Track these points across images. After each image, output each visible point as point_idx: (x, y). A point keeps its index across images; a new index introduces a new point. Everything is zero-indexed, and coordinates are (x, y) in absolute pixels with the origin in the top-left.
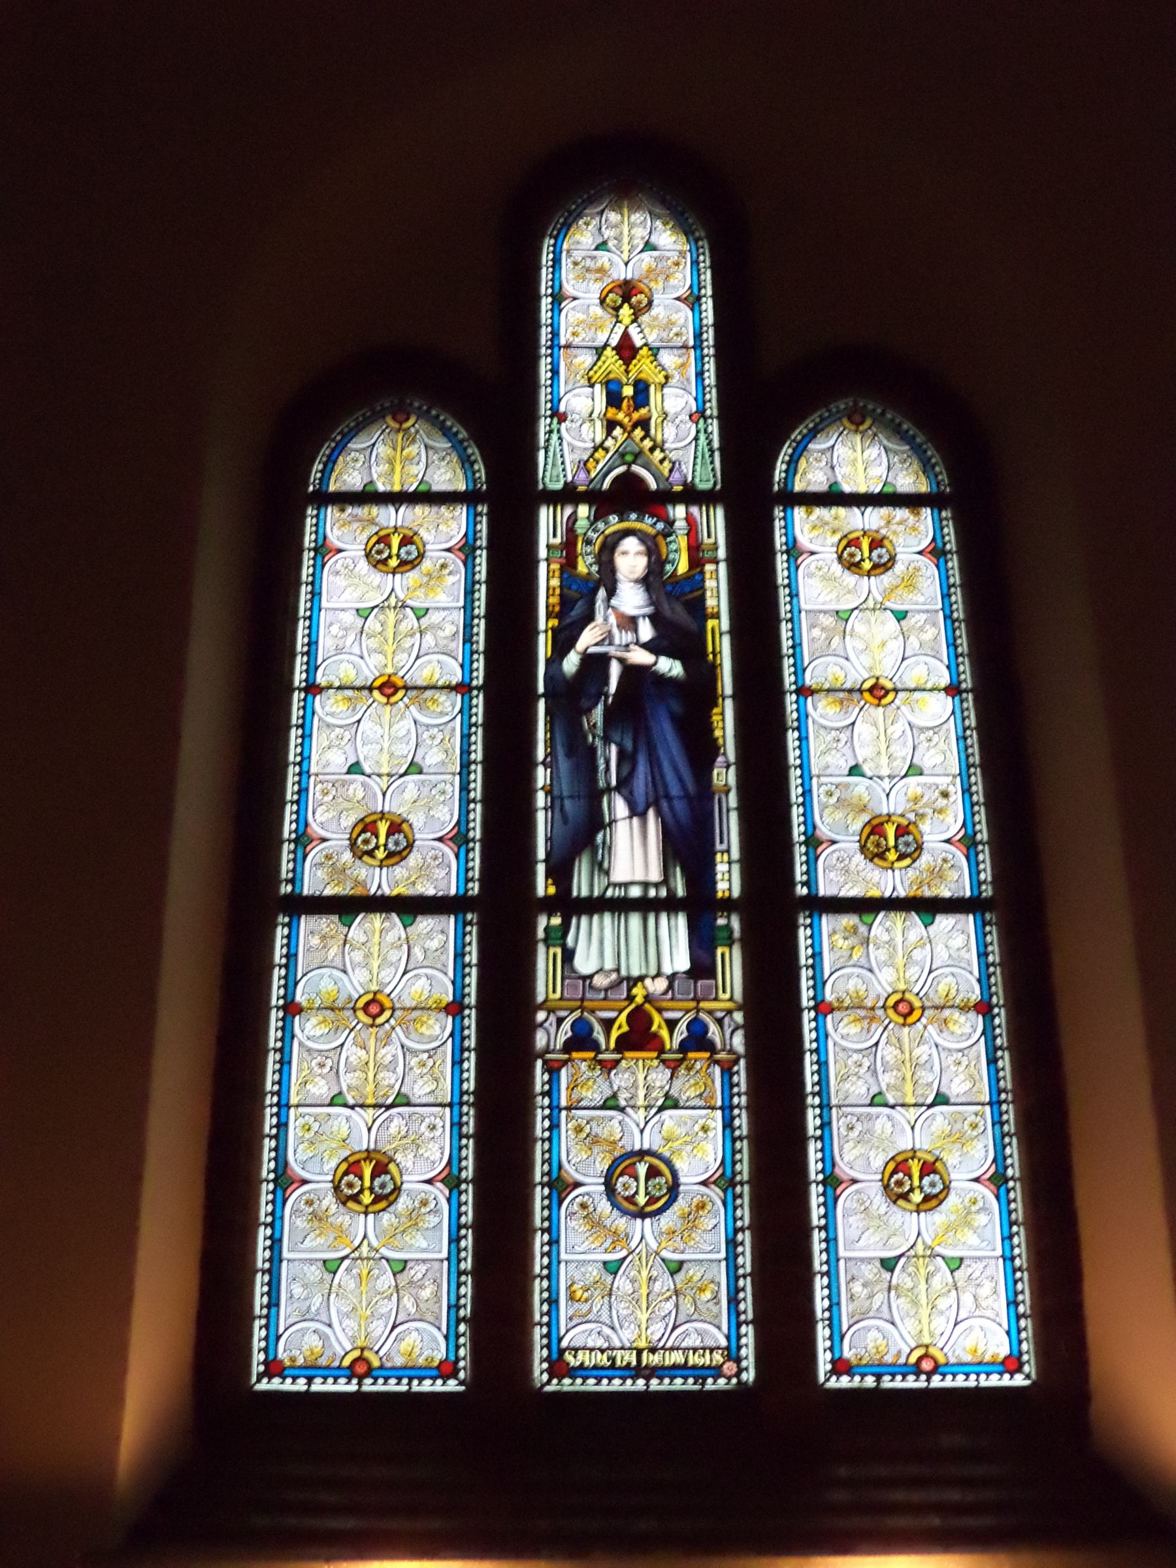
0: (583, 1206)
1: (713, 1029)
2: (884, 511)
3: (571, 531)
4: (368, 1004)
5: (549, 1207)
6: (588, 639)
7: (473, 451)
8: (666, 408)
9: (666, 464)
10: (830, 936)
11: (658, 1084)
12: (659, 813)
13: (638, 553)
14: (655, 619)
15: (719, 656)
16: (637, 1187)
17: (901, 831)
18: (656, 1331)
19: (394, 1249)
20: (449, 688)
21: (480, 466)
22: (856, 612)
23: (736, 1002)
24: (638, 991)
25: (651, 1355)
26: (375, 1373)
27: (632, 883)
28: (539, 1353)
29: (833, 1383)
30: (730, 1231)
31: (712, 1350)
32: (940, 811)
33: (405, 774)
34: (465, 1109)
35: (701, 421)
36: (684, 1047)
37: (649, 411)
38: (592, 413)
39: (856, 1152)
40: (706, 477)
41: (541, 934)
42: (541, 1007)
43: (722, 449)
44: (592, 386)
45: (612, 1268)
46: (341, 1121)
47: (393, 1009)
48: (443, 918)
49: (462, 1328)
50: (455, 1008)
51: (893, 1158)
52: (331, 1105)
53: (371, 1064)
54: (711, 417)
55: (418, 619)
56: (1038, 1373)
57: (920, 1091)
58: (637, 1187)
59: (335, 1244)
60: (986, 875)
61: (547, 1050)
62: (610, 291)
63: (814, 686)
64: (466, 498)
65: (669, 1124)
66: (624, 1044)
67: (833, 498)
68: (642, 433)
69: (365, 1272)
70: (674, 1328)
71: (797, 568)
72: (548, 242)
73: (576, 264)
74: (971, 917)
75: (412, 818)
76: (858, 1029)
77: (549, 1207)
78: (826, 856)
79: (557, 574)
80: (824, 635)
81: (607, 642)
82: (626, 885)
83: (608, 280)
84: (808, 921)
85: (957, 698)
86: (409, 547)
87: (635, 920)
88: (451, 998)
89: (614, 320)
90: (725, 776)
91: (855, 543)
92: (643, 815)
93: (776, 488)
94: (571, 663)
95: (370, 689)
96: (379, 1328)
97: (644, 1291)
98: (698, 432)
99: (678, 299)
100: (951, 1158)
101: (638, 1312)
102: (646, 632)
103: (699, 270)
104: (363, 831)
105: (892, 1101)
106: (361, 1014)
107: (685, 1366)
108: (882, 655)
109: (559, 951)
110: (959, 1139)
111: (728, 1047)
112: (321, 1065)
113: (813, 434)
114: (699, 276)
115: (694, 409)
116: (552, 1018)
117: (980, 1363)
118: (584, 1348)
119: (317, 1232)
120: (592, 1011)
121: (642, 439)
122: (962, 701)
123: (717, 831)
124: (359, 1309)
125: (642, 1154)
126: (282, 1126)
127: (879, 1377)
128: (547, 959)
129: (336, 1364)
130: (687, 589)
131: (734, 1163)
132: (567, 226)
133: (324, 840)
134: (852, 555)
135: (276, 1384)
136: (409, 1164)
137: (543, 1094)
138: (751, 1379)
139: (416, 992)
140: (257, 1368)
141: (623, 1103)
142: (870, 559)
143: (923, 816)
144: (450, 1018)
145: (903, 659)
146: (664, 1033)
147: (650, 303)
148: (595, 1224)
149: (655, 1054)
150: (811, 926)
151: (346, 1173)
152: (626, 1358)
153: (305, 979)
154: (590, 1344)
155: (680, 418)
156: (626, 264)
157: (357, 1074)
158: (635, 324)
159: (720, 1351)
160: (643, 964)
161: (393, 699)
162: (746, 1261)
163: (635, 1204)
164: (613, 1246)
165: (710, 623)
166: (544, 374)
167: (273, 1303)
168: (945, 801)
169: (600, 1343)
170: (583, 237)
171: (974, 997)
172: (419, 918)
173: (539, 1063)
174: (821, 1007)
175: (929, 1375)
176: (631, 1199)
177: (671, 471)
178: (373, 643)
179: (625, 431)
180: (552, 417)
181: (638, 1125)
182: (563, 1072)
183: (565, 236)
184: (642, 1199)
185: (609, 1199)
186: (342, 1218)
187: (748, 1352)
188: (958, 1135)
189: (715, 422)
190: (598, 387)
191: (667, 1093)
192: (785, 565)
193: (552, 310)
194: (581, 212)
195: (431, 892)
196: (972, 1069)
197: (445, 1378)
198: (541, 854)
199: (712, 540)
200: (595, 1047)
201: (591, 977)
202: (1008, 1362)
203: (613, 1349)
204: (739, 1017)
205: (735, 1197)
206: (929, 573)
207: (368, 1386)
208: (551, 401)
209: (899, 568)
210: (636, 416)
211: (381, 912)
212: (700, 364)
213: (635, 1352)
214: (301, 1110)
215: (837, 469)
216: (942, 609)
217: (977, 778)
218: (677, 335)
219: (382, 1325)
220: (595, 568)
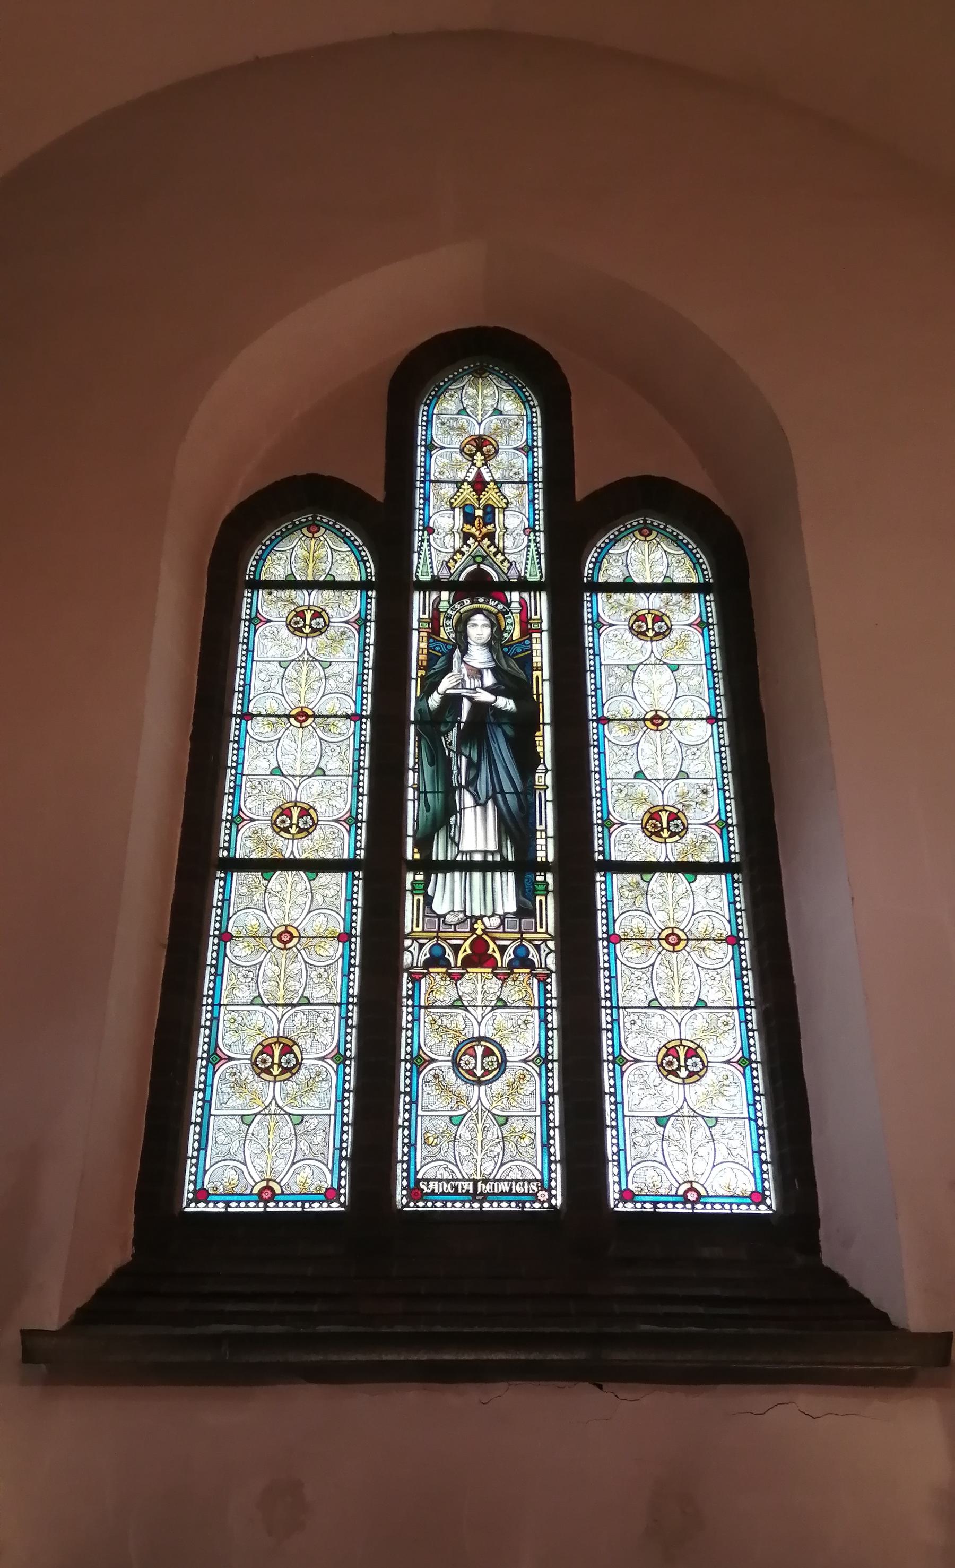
0: (436, 1076)
1: (533, 951)
2: (664, 596)
3: (436, 612)
5: (411, 1078)
6: (446, 684)
7: (366, 552)
8: (506, 525)
9: (506, 564)
10: (619, 889)
12: (496, 803)
13: (484, 625)
15: (541, 696)
16: (476, 1064)
17: (673, 817)
18: (488, 1167)
19: (294, 1107)
20: (347, 716)
21: (370, 564)
22: (641, 666)
24: (479, 926)
25: (484, 1185)
26: (277, 1198)
27: (477, 851)
28: (400, 1183)
29: (621, 1208)
30: (544, 1095)
31: (529, 1181)
32: (702, 803)
33: (313, 775)
34: (350, 1007)
35: (532, 534)
36: (511, 966)
37: (495, 527)
38: (453, 528)
39: (637, 1041)
41: (409, 886)
42: (407, 937)
43: (547, 554)
44: (453, 509)
45: (456, 1121)
46: (258, 1016)
48: (338, 875)
49: (344, 1164)
51: (664, 1046)
52: (252, 1004)
53: (282, 976)
54: (539, 531)
55: (324, 669)
56: (777, 1206)
59: (250, 1104)
60: (736, 848)
61: (412, 967)
62: (467, 444)
64: (362, 586)
65: (499, 1018)
66: (468, 962)
67: (628, 587)
68: (489, 543)
69: (272, 1124)
70: (502, 1165)
71: (599, 635)
73: (443, 424)
74: (723, 876)
75: (317, 806)
76: (639, 954)
77: (411, 1078)
78: (616, 833)
79: (425, 639)
80: (617, 682)
81: (460, 687)
82: (471, 853)
83: (465, 436)
84: (603, 879)
86: (285, 1066)
87: (477, 876)
88: (342, 931)
89: (470, 463)
90: (545, 778)
91: (643, 618)
92: (484, 805)
93: (585, 580)
94: (434, 701)
95: (288, 717)
96: (281, 1165)
97: (480, 1138)
98: (529, 541)
99: (516, 449)
100: (708, 1046)
102: (489, 680)
103: (533, 427)
104: (281, 815)
105: (664, 1005)
106: (275, 941)
107: (510, 1193)
108: (660, 695)
109: (421, 898)
110: (715, 1034)
111: (543, 966)
112: (246, 977)
113: (615, 541)
114: (533, 431)
115: (527, 526)
116: (416, 945)
117: (732, 1196)
118: (434, 1180)
119: (238, 1095)
121: (489, 546)
122: (719, 727)
124: (267, 1151)
125: (480, 1039)
126: (215, 1019)
127: (655, 1204)
128: (413, 902)
129: (248, 1192)
130: (519, 650)
132: (438, 396)
133: (252, 820)
134: (640, 627)
135: (201, 1207)
136: (308, 1047)
137: (408, 997)
142: (653, 629)
143: (688, 806)
145: (676, 698)
146: (497, 955)
147: (497, 452)
148: (444, 1089)
149: (490, 970)
150: (605, 882)
151: (261, 1053)
152: (466, 1187)
153: (235, 916)
154: (439, 1177)
155: (516, 532)
156: (480, 424)
158: (485, 467)
159: (535, 1183)
160: (482, 907)
161: (304, 724)
162: (556, 1117)
163: (475, 1075)
164: (456, 1105)
165: (535, 674)
166: (419, 501)
167: (203, 1147)
168: (705, 797)
169: (446, 1176)
170: (448, 406)
171: (725, 933)
172: (320, 875)
173: (405, 975)
174: (612, 939)
175: (694, 1203)
176: (471, 1072)
177: (509, 569)
178: (290, 686)
179: (476, 541)
180: (423, 531)
181: (477, 1020)
182: (423, 981)
183: (435, 405)
184: (479, 1072)
186: (258, 1085)
187: (557, 1184)
188: (713, 1030)
189: (542, 535)
190: (457, 510)
191: (499, 997)
192: (591, 634)
193: (425, 457)
195: (330, 857)
198: (410, 831)
199: (538, 617)
200: (447, 964)
201: (444, 916)
202: (754, 1197)
203: (458, 1180)
204: (551, 944)
205: (548, 1070)
207: (272, 1207)
208: (423, 520)
209: (674, 635)
210: (484, 530)
213: (471, 1183)
214: (228, 1008)
215: (630, 568)
217: (729, 780)
219: (284, 1163)
220: (453, 635)
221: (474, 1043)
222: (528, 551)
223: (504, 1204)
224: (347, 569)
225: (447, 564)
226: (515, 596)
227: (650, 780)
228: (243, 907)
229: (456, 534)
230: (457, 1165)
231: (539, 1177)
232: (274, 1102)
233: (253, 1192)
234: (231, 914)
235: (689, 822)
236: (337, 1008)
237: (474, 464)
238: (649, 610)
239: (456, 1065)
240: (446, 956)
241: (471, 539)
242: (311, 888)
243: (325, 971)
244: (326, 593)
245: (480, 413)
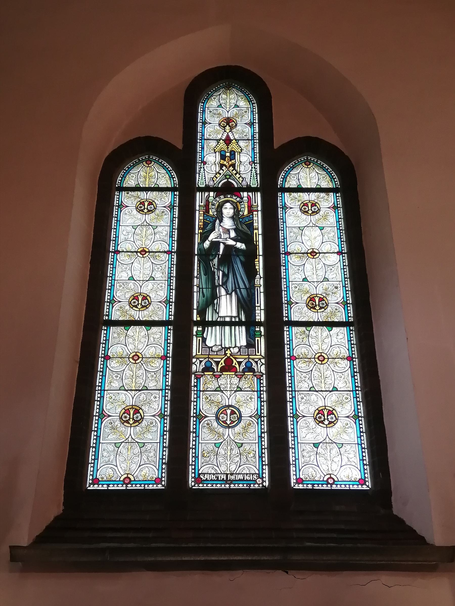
0: (208, 424)
1: (254, 364)
3: (207, 201)
4: (133, 356)
6: (212, 237)
7: (174, 173)
9: (241, 179)
11: (234, 383)
12: (236, 293)
13: (230, 208)
14: (236, 230)
17: (321, 300)
18: (233, 467)
19: (140, 439)
20: (165, 252)
21: (176, 179)
22: (306, 228)
23: (262, 356)
24: (228, 352)
26: (132, 482)
27: (227, 316)
28: (191, 475)
29: (296, 487)
30: (260, 433)
31: (253, 474)
32: (335, 293)
36: (244, 371)
37: (235, 161)
38: (215, 162)
39: (304, 407)
40: (254, 184)
41: (195, 333)
42: (194, 357)
44: (215, 153)
45: (217, 445)
46: (123, 396)
47: (143, 358)
48: (161, 328)
52: (120, 390)
53: (134, 376)
54: (257, 163)
55: (154, 229)
57: (327, 386)
60: (351, 314)
63: (291, 252)
66: (223, 369)
67: (299, 190)
68: (233, 169)
69: (130, 447)
72: (201, 104)
73: (210, 112)
74: (345, 328)
75: (151, 295)
82: (224, 317)
83: (221, 118)
84: (288, 329)
85: (341, 256)
86: (151, 206)
87: (227, 328)
90: (260, 281)
91: (306, 205)
92: (231, 294)
94: (207, 244)
95: (137, 252)
96: (134, 467)
97: (229, 454)
98: (252, 168)
99: (246, 124)
100: (338, 409)
101: (227, 461)
102: (233, 234)
103: (253, 113)
104: (133, 299)
107: (243, 480)
108: (315, 242)
109: (201, 339)
112: (117, 377)
116: (198, 361)
117: (350, 481)
118: (207, 474)
121: (232, 171)
122: (343, 256)
125: (229, 406)
126: (102, 397)
129: (118, 479)
130: (247, 220)
131: (261, 409)
133: (120, 302)
134: (305, 209)
135: (96, 487)
136: (147, 410)
138: (267, 485)
139: (151, 352)
140: (89, 481)
141: (222, 389)
142: (311, 210)
144: (162, 361)
145: (322, 243)
146: (237, 366)
147: (236, 125)
148: (212, 430)
151: (124, 413)
152: (222, 477)
153: (111, 348)
154: (210, 472)
156: (228, 112)
157: (129, 380)
158: (231, 132)
159: (256, 475)
160: (230, 343)
161: (144, 256)
163: (226, 423)
164: (218, 438)
165: (255, 231)
166: (199, 149)
167: (96, 458)
168: (336, 290)
169: (213, 472)
170: (213, 103)
171: (346, 355)
173: (193, 376)
176: (225, 422)
177: (242, 181)
179: (226, 168)
181: (227, 397)
182: (202, 378)
183: (207, 103)
184: (228, 422)
185: (217, 422)
187: (266, 475)
188: (341, 402)
189: (258, 165)
190: (217, 153)
192: (281, 212)
194: (212, 95)
195: (157, 319)
196: (346, 379)
197: (157, 484)
198: (195, 307)
200: (213, 370)
201: (212, 347)
203: (219, 474)
204: (263, 361)
206: (332, 214)
207: (129, 487)
208: (201, 158)
209: (321, 213)
210: (230, 163)
211: (139, 325)
212: (253, 145)
214: (108, 392)
215: (300, 180)
216: (337, 226)
217: (348, 282)
218: (245, 136)
220: (215, 213)
221: (226, 408)
225: (212, 179)
226: (245, 194)
227: (310, 282)
230: (218, 467)
231: (257, 472)
233: (121, 480)
236: (161, 392)
239: (217, 419)
241: (224, 167)
243: (155, 374)
245: (228, 107)
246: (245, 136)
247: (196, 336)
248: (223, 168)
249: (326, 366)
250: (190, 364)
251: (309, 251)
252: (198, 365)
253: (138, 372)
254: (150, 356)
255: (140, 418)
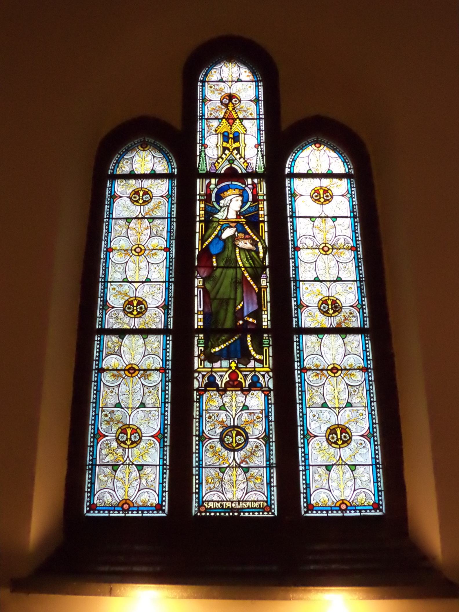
1: (261, 378)
7: (172, 157)
37: (240, 144)
38: (217, 144)
40: (261, 171)
48: (159, 336)
50: (167, 250)
58: (232, 440)
62: (224, 98)
68: (237, 152)
86: (141, 306)
98: (258, 151)
111: (267, 386)
116: (200, 375)
120: (216, 372)
121: (236, 154)
123: (263, 299)
125: (234, 427)
154: (214, 500)
169: (218, 499)
182: (205, 395)
196: (350, 269)
203: (224, 501)
221: (231, 429)
222: (257, 156)
223: (247, 514)
224: (162, 167)
225: (214, 165)
226: (249, 181)
227: (330, 408)
228: (116, 236)
229: (219, 147)
230: (223, 494)
231: (265, 499)
232: (128, 459)
233: (119, 505)
234: (112, 239)
235: (343, 305)
236: (164, 284)
237: (228, 109)
238: (321, 187)
239: (222, 441)
240: (217, 381)
241: (227, 150)
242: (140, 475)
243: (152, 389)
244: (150, 181)
245: (234, 408)
246: (250, 114)
247: (198, 313)
248: (226, 152)
249: (330, 256)
250: (191, 379)
251: (330, 368)
252: (201, 380)
253: (135, 387)
254: (152, 248)
255: (138, 438)
